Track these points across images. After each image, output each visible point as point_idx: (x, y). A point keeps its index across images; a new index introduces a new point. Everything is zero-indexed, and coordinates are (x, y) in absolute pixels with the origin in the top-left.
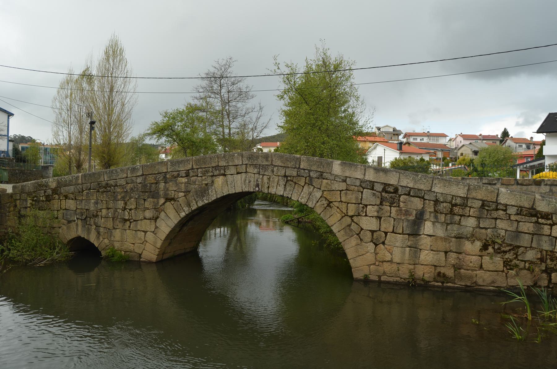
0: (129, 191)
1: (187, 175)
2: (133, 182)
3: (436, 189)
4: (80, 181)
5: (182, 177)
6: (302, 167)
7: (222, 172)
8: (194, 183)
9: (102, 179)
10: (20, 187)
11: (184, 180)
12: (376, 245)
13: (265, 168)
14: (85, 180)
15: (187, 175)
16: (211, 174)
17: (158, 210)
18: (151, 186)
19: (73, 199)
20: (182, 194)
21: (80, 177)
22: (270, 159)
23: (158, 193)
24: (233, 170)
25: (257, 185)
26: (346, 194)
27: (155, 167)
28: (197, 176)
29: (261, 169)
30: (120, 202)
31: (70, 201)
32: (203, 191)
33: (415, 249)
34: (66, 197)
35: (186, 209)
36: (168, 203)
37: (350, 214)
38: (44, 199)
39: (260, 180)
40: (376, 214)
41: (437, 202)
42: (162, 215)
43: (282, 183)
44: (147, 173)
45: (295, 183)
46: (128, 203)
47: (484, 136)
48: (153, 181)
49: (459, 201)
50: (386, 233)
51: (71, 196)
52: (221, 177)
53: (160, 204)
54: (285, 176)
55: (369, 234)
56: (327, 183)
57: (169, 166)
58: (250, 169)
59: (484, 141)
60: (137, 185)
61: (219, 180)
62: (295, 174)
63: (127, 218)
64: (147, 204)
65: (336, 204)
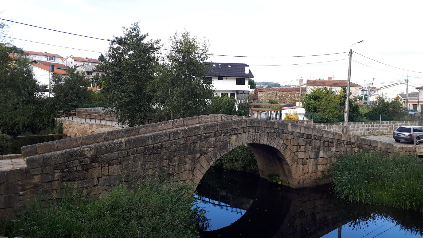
0: (173, 151)
1: (215, 135)
2: (176, 143)
3: (324, 136)
4: (124, 147)
5: (212, 137)
6: (275, 127)
7: (236, 132)
8: (219, 140)
9: (147, 143)
10: (42, 160)
11: (213, 139)
12: (303, 165)
13: (258, 128)
14: (130, 145)
15: (215, 135)
16: (229, 134)
17: (194, 161)
18: (190, 146)
19: (118, 165)
20: (212, 149)
21: (124, 144)
22: (260, 123)
23: (195, 150)
24: (242, 131)
25: (254, 139)
26: (293, 141)
27: (193, 131)
28: (221, 136)
29: (257, 129)
30: (165, 161)
31: (114, 166)
32: (225, 146)
33: (317, 165)
34: (109, 164)
35: (214, 159)
36: (202, 157)
37: (294, 151)
38: (79, 169)
39: (256, 136)
40: (304, 150)
41: (324, 141)
42: (198, 165)
43: (266, 137)
44: (186, 136)
45: (272, 137)
46: (173, 161)
47: (89, 59)
48: (192, 142)
49: (331, 141)
50: (307, 159)
51: (116, 162)
52: (235, 136)
53: (197, 158)
54: (268, 133)
55: (301, 160)
56: (286, 136)
57: (202, 130)
58: (251, 130)
59: (90, 64)
60: (180, 146)
61: (234, 138)
62: (272, 131)
63: (171, 173)
64: (187, 160)
65: (289, 146)
